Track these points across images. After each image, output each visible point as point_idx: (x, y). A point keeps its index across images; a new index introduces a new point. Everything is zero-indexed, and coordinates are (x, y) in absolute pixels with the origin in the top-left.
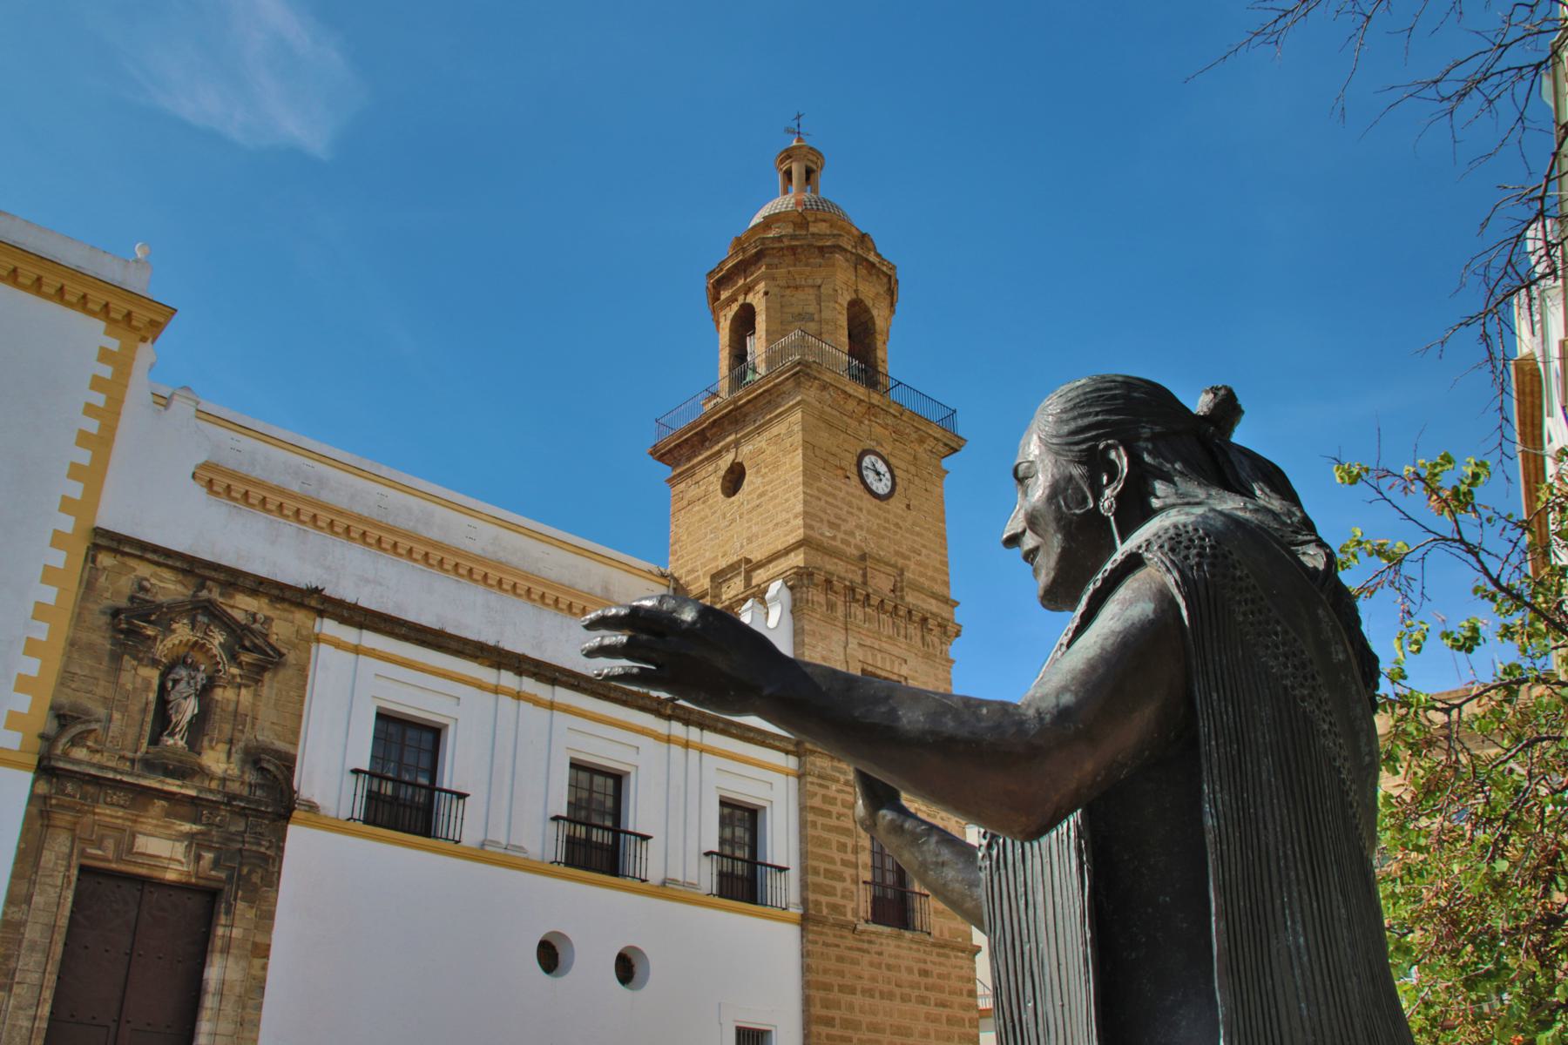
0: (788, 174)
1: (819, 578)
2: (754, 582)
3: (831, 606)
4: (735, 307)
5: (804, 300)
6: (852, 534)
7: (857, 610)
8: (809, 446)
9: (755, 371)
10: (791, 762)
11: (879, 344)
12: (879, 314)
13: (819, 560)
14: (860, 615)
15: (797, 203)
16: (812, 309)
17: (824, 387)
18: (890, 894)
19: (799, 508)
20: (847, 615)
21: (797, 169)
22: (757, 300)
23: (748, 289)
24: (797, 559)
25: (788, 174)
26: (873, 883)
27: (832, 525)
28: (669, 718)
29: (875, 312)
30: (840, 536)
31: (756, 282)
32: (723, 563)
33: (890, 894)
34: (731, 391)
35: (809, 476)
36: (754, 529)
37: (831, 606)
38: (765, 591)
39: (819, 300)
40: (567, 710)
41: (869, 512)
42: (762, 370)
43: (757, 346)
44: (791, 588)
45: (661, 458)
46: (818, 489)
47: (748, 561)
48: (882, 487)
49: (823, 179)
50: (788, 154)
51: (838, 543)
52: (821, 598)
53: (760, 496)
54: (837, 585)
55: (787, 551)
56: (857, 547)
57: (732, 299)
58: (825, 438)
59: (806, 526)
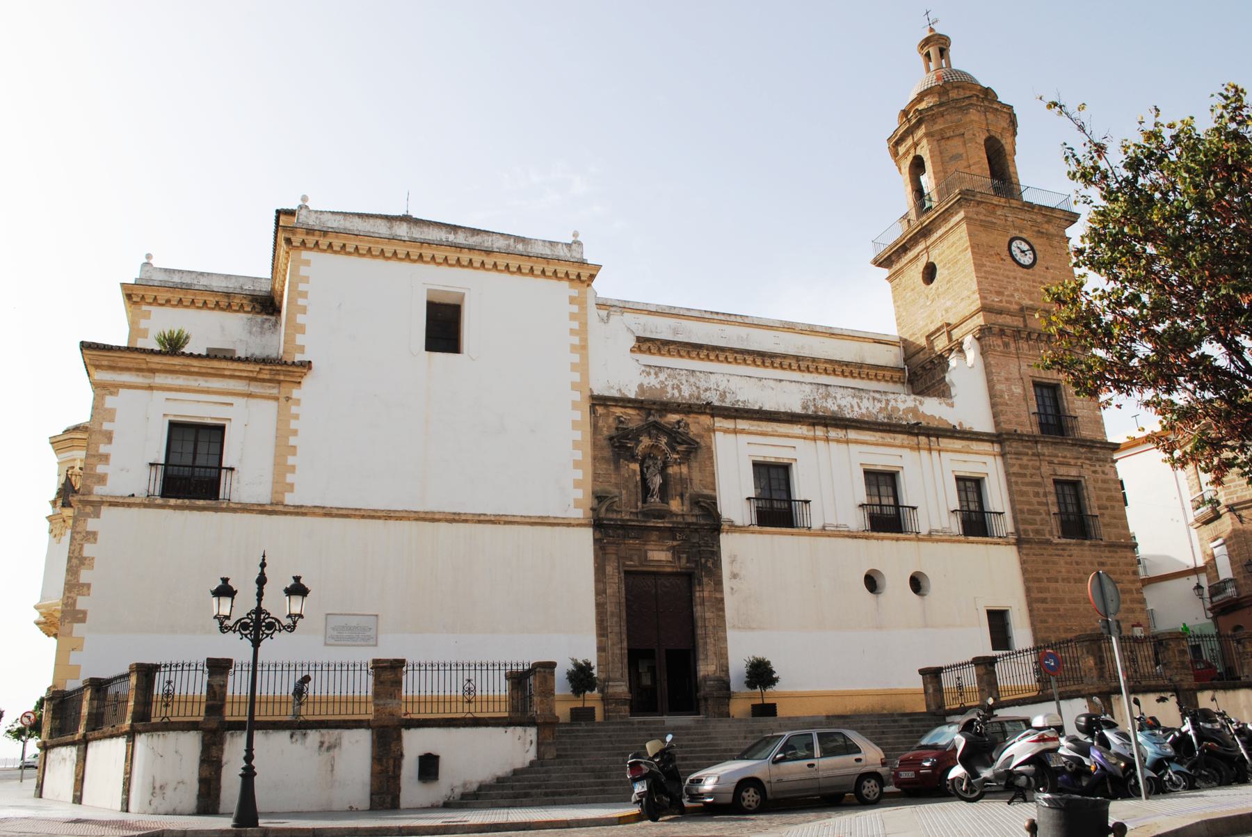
0: (928, 55)
1: (996, 329)
2: (954, 338)
3: (1006, 345)
4: (910, 158)
5: (955, 146)
6: (1012, 296)
7: (1024, 345)
8: (976, 247)
9: (930, 200)
10: (997, 448)
11: (1010, 163)
12: (1006, 142)
13: (993, 317)
14: (1026, 346)
15: (938, 78)
16: (961, 150)
17: (979, 203)
18: (1051, 420)
19: (975, 287)
20: (1017, 349)
21: (933, 51)
22: (924, 151)
23: (916, 145)
24: (979, 320)
25: (928, 55)
26: (1039, 414)
27: (999, 293)
28: (917, 435)
29: (1003, 142)
30: (1004, 299)
31: (920, 139)
32: (933, 329)
33: (1051, 420)
34: (918, 217)
35: (978, 267)
36: (949, 304)
37: (1006, 345)
38: (962, 343)
39: (965, 144)
40: (856, 442)
41: (1021, 279)
42: (935, 198)
43: (928, 181)
44: (978, 339)
45: (880, 265)
46: (986, 272)
47: (948, 325)
48: (1027, 260)
49: (953, 52)
50: (927, 42)
51: (1004, 304)
52: (999, 342)
53: (949, 282)
54: (1008, 332)
55: (971, 316)
56: (1017, 303)
57: (907, 152)
58: (984, 237)
59: (982, 298)
